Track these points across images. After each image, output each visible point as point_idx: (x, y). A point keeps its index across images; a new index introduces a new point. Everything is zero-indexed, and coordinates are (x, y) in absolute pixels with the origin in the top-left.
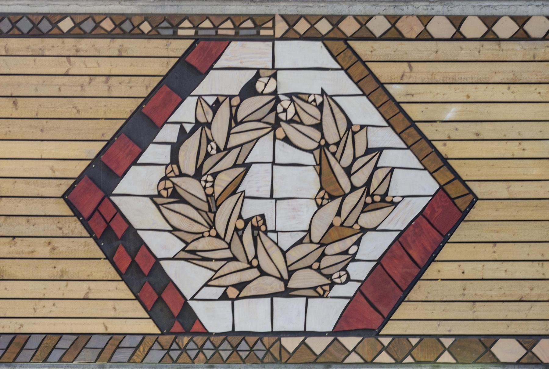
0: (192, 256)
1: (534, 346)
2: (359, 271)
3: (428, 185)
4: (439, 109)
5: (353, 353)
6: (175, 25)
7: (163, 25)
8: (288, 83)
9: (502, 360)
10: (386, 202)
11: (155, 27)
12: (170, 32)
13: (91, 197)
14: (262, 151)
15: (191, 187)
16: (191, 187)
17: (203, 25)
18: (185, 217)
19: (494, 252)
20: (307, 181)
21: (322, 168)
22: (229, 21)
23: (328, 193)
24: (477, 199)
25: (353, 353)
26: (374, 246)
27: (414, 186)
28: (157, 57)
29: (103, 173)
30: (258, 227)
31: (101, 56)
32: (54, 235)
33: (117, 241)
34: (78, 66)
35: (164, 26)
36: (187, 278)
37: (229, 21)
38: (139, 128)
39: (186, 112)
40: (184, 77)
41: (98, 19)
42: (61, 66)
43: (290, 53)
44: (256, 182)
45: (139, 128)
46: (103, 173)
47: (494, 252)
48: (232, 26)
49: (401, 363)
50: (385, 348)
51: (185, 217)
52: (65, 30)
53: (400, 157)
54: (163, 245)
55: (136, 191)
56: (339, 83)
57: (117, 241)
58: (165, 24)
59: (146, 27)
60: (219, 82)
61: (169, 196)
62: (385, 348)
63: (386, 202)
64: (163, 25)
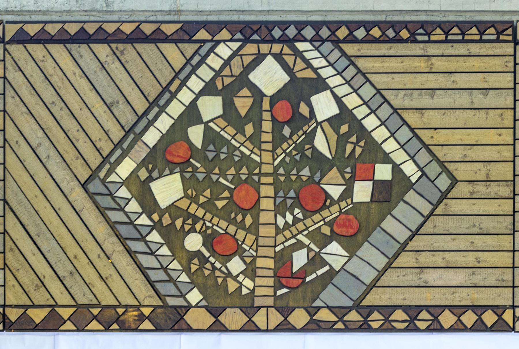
1: (35, 323)
5: (68, 321)
6: (500, 31)
7: (418, 32)
9: (302, 309)
11: (413, 34)
12: (426, 38)
17: (453, 31)
22: (474, 28)
24: (457, 181)
25: (68, 321)
32: (51, 230)
37: (474, 28)
41: (352, 27)
48: (477, 32)
49: (83, 330)
50: (95, 317)
52: (360, 37)
58: (421, 31)
59: (404, 34)
62: (95, 317)
64: (418, 32)
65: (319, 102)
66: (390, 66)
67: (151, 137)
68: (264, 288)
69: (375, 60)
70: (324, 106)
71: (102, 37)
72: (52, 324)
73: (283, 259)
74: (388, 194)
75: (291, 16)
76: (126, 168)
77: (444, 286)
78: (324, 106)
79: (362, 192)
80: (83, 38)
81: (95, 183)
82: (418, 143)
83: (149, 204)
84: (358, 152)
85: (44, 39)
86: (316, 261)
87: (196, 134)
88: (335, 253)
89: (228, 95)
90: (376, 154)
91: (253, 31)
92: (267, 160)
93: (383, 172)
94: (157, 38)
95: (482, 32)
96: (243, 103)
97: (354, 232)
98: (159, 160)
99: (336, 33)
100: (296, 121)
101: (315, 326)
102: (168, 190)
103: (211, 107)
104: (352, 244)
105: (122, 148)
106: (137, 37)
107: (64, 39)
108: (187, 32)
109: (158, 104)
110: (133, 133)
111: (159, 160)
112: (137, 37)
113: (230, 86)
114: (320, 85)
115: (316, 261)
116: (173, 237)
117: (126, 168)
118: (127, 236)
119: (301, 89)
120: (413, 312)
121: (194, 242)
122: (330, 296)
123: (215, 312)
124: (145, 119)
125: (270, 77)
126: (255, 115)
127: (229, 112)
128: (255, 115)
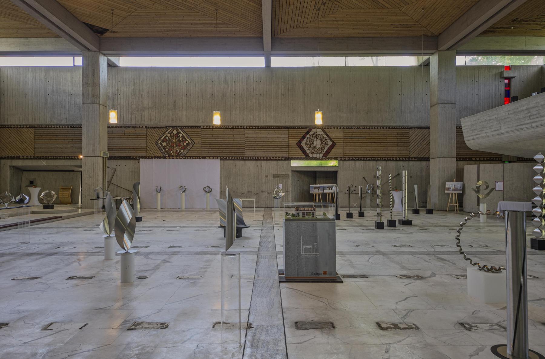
0: (309, 150)
2: (325, 151)
3: (331, 143)
4: (333, 136)
8: (318, 133)
10: (327, 144)
13: (299, 144)
14: (315, 140)
15: (309, 143)
16: (309, 143)
18: (308, 146)
19: (267, 176)
20: (319, 142)
21: (321, 141)
23: (322, 143)
26: (326, 149)
27: (330, 143)
28: (305, 131)
29: (300, 142)
30: (315, 147)
31: (300, 131)
33: (302, 148)
34: (298, 12)
35: (306, 128)
36: (308, 152)
38: (304, 137)
39: (308, 136)
40: (308, 133)
42: (289, 22)
43: (318, 130)
44: (315, 143)
45: (304, 137)
46: (300, 142)
47: (267, 176)
51: (308, 146)
53: (328, 140)
54: (306, 149)
55: (303, 143)
56: (323, 133)
57: (302, 148)
60: (311, 133)
61: (306, 144)
63: (327, 144)
65: (246, 89)
66: (188, 131)
67: (162, 138)
68: (174, 154)
69: (186, 130)
70: (181, 135)
71: (157, 128)
72: (152, 158)
73: (177, 151)
74: (188, 144)
75: (437, 193)
76: (160, 142)
77: (194, 154)
78: (181, 135)
79: (185, 144)
80: (155, 128)
81: (156, 143)
82: (191, 139)
83: (162, 145)
84: (184, 140)
85: (151, 128)
86: (180, 152)
87: (167, 138)
88: (182, 151)
89: (170, 134)
90: (186, 140)
91: (173, 127)
92: (175, 141)
93: (187, 142)
94: (163, 128)
95: (512, 95)
96: (172, 135)
97: (184, 148)
98: (163, 141)
99: (182, 127)
100: (178, 137)
101: (180, 158)
102: (164, 144)
103: (169, 135)
104: (184, 150)
105: (159, 139)
106: (161, 128)
107: (153, 128)
108: (166, 127)
109: (163, 135)
110: (160, 138)
111: (163, 141)
112: (161, 128)
113: (171, 133)
114: (180, 133)
115: (180, 152)
116: (165, 149)
117: (160, 142)
118: (160, 149)
119: (178, 133)
120: (190, 157)
121: (167, 150)
122: (182, 155)
123: (169, 157)
124: (162, 136)
125: (175, 132)
126: (173, 136)
127: (171, 136)
128: (173, 136)
